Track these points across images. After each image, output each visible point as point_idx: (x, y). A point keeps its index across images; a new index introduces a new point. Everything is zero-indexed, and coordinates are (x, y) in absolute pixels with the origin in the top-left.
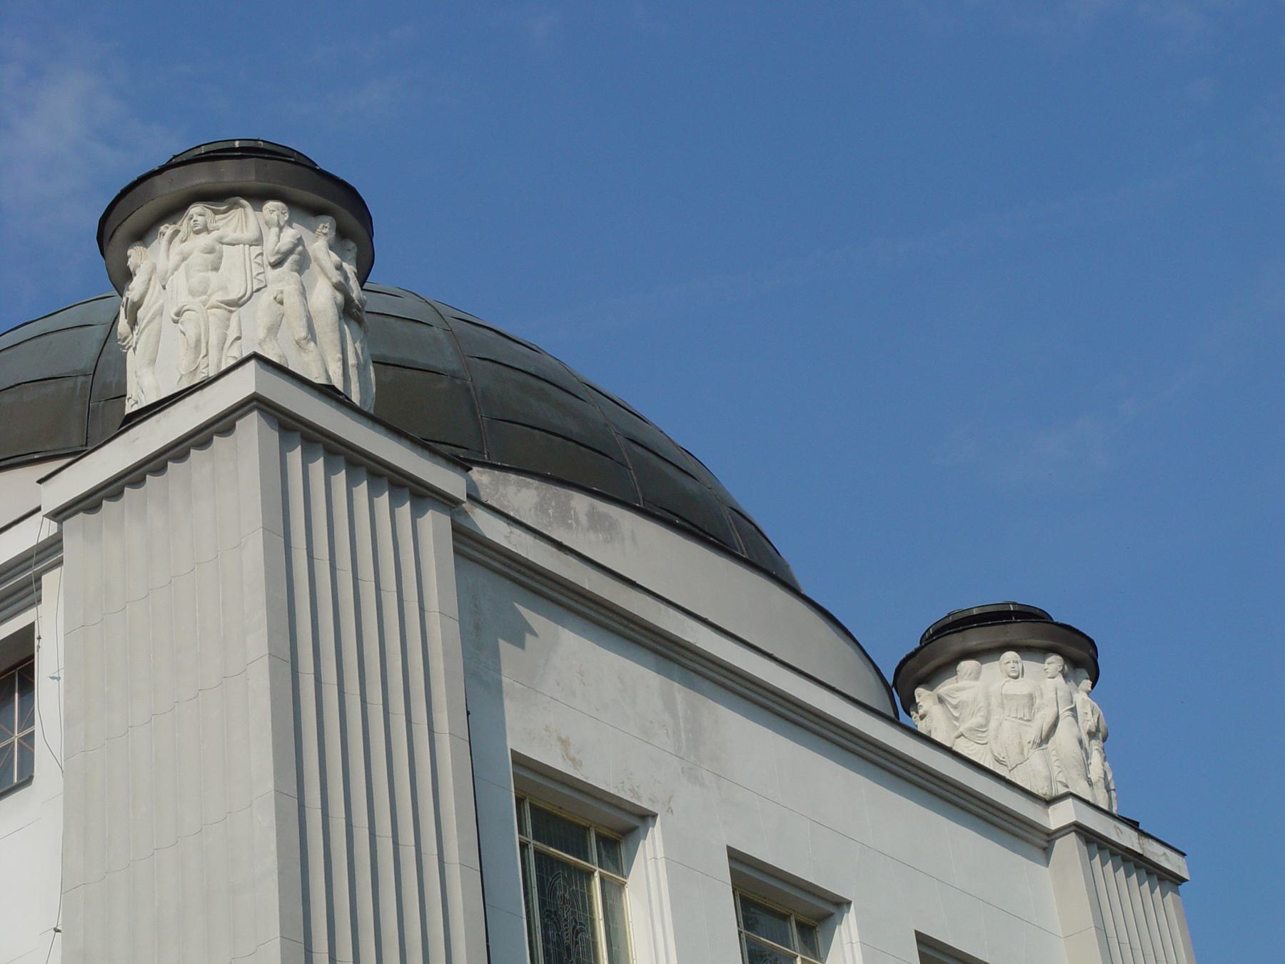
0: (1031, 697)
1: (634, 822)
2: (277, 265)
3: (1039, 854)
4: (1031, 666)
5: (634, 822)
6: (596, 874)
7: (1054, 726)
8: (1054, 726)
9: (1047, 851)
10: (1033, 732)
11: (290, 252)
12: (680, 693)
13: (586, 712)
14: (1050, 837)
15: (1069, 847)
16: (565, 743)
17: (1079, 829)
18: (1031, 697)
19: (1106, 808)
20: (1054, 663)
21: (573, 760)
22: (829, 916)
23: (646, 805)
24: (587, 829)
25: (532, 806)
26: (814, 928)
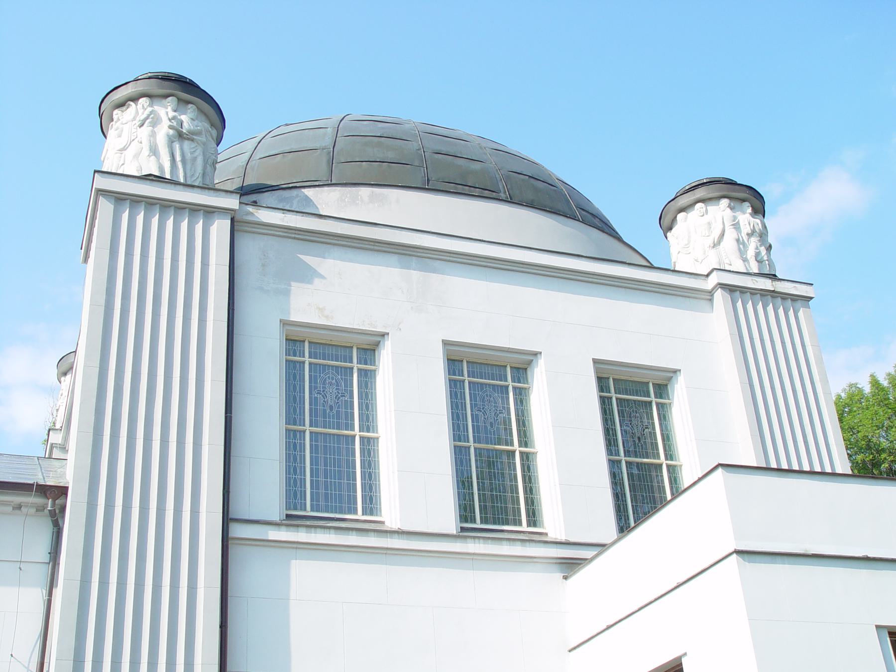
0: (709, 224)
1: (378, 339)
2: (141, 126)
3: (705, 304)
4: (712, 209)
5: (378, 339)
6: (510, 389)
7: (722, 235)
8: (722, 235)
9: (711, 300)
10: (710, 242)
11: (147, 118)
12: (415, 275)
13: (335, 295)
14: (711, 293)
15: (719, 294)
16: (321, 310)
17: (723, 286)
18: (709, 224)
19: (745, 271)
20: (725, 202)
21: (327, 317)
22: (377, 344)
23: (380, 329)
24: (648, 383)
25: (614, 380)
26: (526, 369)
